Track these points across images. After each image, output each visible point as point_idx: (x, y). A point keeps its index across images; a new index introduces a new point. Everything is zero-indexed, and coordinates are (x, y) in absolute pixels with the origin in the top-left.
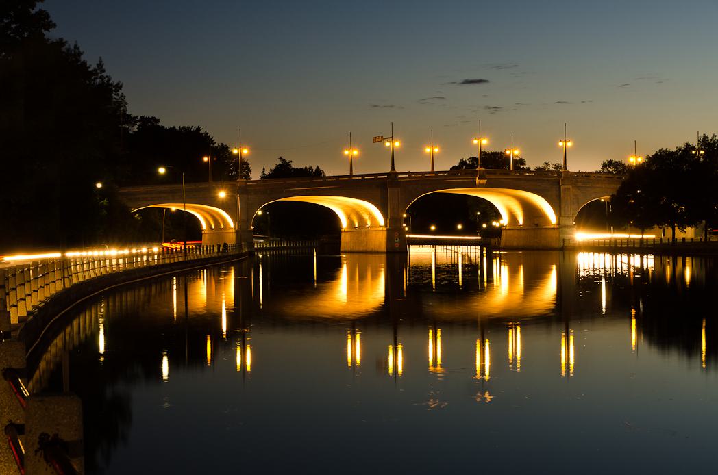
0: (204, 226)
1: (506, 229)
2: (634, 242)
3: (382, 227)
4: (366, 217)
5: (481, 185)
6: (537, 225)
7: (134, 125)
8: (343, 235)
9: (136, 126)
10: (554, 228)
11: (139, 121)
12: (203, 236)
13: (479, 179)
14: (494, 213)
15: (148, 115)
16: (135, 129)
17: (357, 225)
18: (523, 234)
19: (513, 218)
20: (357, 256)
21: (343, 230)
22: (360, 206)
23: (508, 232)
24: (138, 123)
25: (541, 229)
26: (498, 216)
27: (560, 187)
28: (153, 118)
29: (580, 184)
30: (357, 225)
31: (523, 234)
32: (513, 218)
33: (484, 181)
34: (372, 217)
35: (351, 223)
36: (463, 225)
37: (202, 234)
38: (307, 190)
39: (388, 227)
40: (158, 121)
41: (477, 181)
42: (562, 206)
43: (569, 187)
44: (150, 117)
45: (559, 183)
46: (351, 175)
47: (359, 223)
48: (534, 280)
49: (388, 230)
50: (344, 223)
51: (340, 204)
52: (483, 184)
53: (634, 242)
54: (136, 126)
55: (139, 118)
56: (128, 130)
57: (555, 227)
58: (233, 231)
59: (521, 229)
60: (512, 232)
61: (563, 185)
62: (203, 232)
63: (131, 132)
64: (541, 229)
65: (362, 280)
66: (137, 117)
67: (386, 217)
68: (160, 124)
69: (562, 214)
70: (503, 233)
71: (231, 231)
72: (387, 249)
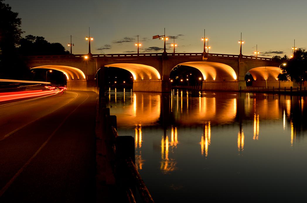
0: (68, 78)
1: (205, 82)
2: (285, 89)
3: (159, 79)
4: (149, 75)
5: (205, 61)
6: (224, 80)
7: (34, 40)
8: (134, 84)
9: (35, 40)
10: (235, 82)
11: (36, 38)
12: (67, 83)
13: (204, 57)
14: (200, 74)
15: (40, 36)
16: (35, 41)
17: (143, 79)
18: (215, 84)
19: (210, 77)
20: (140, 93)
21: (134, 81)
22: (146, 69)
23: (206, 83)
24: (36, 39)
25: (227, 82)
26: (201, 75)
27: (239, 62)
28: (42, 37)
29: (247, 62)
30: (143, 79)
31: (215, 84)
32: (210, 77)
33: (206, 59)
34: (153, 75)
35: (139, 77)
36: (125, 82)
37: (66, 82)
38: (120, 61)
39: (163, 79)
40: (44, 38)
41: (203, 58)
42: (240, 71)
43: (242, 62)
44: (41, 37)
45: (238, 60)
46: (138, 54)
47: (144, 78)
48: (221, 106)
49: (162, 81)
50: (135, 77)
51: (135, 68)
52: (206, 60)
53: (285, 89)
54: (35, 40)
55: (36, 37)
56: (31, 42)
57: (136, 81)
58: (85, 80)
59: (214, 82)
60: (208, 83)
61: (240, 61)
62: (67, 81)
63: (33, 42)
64: (227, 82)
65: (146, 106)
66: (35, 37)
67: (161, 75)
68: (44, 40)
69: (240, 75)
70: (204, 84)
71: (84, 80)
72: (162, 90)
